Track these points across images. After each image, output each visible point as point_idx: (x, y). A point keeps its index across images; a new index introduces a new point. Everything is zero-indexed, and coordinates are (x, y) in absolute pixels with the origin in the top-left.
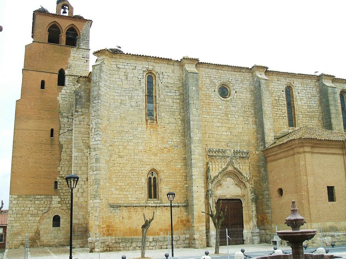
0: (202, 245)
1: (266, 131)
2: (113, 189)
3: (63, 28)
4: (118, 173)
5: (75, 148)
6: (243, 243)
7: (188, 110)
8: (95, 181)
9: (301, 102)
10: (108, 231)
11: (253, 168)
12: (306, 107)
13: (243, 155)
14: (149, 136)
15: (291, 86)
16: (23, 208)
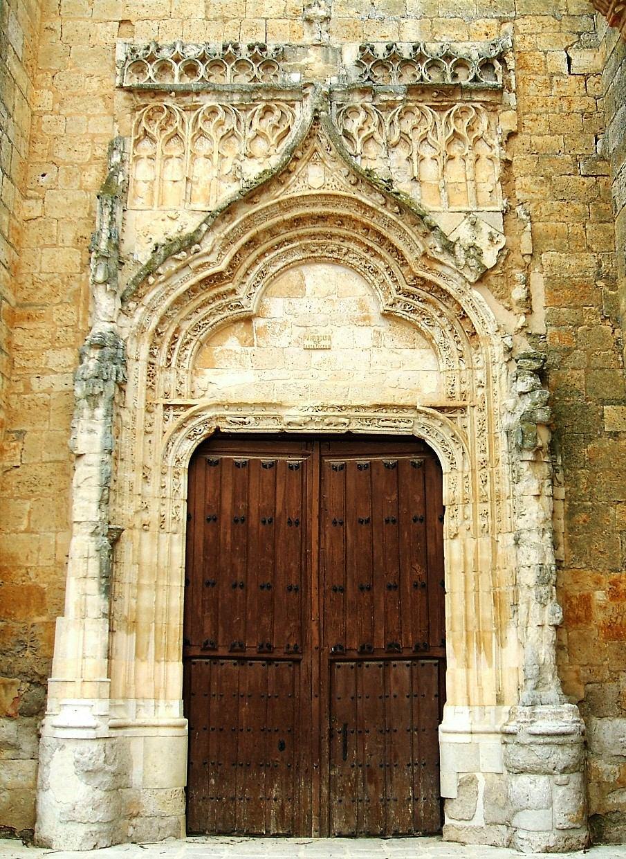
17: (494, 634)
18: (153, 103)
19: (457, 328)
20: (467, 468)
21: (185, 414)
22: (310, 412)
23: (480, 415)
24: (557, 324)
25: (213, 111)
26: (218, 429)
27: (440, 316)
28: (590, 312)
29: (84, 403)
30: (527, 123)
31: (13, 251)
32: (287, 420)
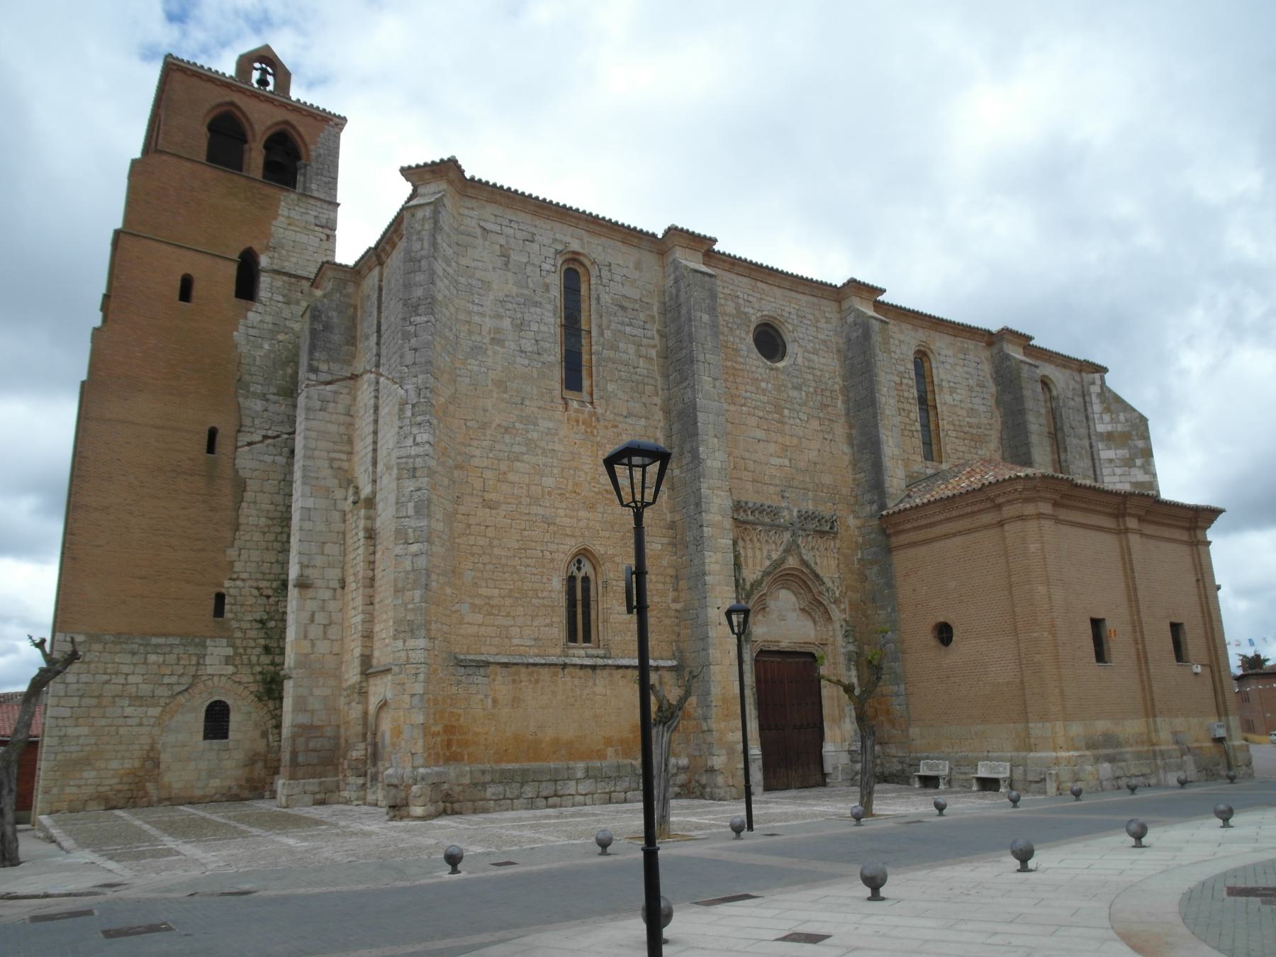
0: (733, 789)
1: (888, 462)
2: (465, 608)
3: (256, 127)
4: (480, 556)
5: (304, 483)
6: (824, 784)
7: (686, 379)
8: (412, 576)
9: (950, 397)
10: (449, 744)
12: (964, 413)
13: (821, 525)
14: (571, 449)
15: (928, 351)
16: (106, 677)
18: (744, 526)
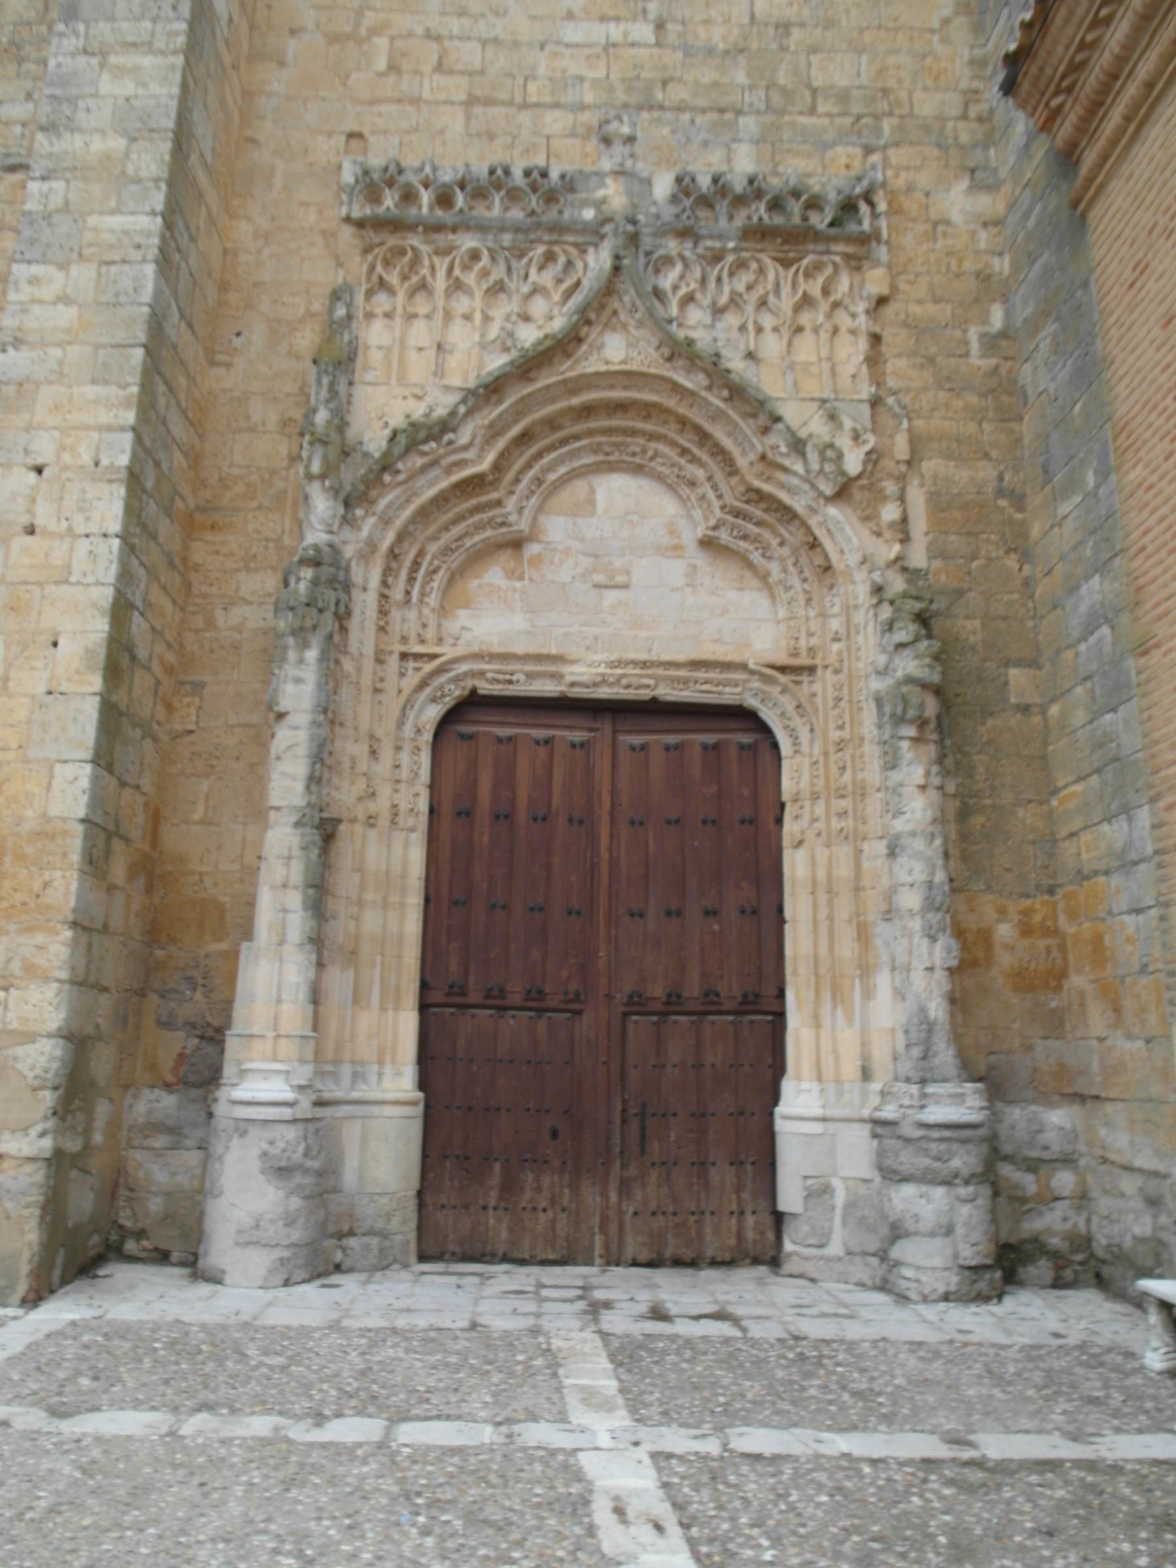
11: (931, 360)
17: (857, 981)
18: (392, 241)
19: (804, 560)
20: (817, 750)
21: (428, 667)
22: (602, 669)
23: (836, 678)
24: (944, 556)
25: (475, 256)
26: (474, 691)
27: (781, 544)
28: (988, 541)
29: (291, 641)
30: (902, 286)
31: (192, 431)
32: (569, 679)
